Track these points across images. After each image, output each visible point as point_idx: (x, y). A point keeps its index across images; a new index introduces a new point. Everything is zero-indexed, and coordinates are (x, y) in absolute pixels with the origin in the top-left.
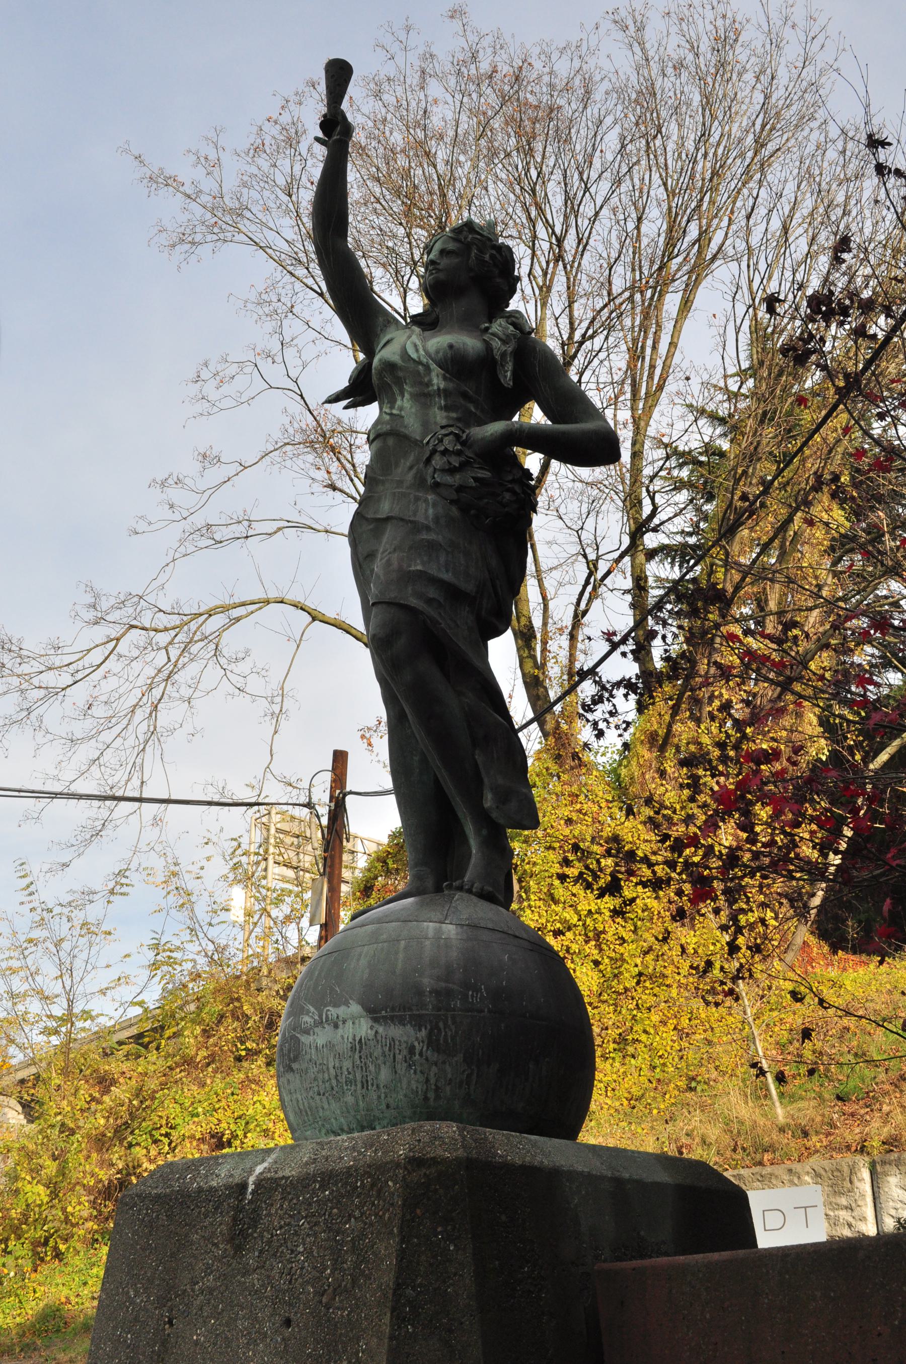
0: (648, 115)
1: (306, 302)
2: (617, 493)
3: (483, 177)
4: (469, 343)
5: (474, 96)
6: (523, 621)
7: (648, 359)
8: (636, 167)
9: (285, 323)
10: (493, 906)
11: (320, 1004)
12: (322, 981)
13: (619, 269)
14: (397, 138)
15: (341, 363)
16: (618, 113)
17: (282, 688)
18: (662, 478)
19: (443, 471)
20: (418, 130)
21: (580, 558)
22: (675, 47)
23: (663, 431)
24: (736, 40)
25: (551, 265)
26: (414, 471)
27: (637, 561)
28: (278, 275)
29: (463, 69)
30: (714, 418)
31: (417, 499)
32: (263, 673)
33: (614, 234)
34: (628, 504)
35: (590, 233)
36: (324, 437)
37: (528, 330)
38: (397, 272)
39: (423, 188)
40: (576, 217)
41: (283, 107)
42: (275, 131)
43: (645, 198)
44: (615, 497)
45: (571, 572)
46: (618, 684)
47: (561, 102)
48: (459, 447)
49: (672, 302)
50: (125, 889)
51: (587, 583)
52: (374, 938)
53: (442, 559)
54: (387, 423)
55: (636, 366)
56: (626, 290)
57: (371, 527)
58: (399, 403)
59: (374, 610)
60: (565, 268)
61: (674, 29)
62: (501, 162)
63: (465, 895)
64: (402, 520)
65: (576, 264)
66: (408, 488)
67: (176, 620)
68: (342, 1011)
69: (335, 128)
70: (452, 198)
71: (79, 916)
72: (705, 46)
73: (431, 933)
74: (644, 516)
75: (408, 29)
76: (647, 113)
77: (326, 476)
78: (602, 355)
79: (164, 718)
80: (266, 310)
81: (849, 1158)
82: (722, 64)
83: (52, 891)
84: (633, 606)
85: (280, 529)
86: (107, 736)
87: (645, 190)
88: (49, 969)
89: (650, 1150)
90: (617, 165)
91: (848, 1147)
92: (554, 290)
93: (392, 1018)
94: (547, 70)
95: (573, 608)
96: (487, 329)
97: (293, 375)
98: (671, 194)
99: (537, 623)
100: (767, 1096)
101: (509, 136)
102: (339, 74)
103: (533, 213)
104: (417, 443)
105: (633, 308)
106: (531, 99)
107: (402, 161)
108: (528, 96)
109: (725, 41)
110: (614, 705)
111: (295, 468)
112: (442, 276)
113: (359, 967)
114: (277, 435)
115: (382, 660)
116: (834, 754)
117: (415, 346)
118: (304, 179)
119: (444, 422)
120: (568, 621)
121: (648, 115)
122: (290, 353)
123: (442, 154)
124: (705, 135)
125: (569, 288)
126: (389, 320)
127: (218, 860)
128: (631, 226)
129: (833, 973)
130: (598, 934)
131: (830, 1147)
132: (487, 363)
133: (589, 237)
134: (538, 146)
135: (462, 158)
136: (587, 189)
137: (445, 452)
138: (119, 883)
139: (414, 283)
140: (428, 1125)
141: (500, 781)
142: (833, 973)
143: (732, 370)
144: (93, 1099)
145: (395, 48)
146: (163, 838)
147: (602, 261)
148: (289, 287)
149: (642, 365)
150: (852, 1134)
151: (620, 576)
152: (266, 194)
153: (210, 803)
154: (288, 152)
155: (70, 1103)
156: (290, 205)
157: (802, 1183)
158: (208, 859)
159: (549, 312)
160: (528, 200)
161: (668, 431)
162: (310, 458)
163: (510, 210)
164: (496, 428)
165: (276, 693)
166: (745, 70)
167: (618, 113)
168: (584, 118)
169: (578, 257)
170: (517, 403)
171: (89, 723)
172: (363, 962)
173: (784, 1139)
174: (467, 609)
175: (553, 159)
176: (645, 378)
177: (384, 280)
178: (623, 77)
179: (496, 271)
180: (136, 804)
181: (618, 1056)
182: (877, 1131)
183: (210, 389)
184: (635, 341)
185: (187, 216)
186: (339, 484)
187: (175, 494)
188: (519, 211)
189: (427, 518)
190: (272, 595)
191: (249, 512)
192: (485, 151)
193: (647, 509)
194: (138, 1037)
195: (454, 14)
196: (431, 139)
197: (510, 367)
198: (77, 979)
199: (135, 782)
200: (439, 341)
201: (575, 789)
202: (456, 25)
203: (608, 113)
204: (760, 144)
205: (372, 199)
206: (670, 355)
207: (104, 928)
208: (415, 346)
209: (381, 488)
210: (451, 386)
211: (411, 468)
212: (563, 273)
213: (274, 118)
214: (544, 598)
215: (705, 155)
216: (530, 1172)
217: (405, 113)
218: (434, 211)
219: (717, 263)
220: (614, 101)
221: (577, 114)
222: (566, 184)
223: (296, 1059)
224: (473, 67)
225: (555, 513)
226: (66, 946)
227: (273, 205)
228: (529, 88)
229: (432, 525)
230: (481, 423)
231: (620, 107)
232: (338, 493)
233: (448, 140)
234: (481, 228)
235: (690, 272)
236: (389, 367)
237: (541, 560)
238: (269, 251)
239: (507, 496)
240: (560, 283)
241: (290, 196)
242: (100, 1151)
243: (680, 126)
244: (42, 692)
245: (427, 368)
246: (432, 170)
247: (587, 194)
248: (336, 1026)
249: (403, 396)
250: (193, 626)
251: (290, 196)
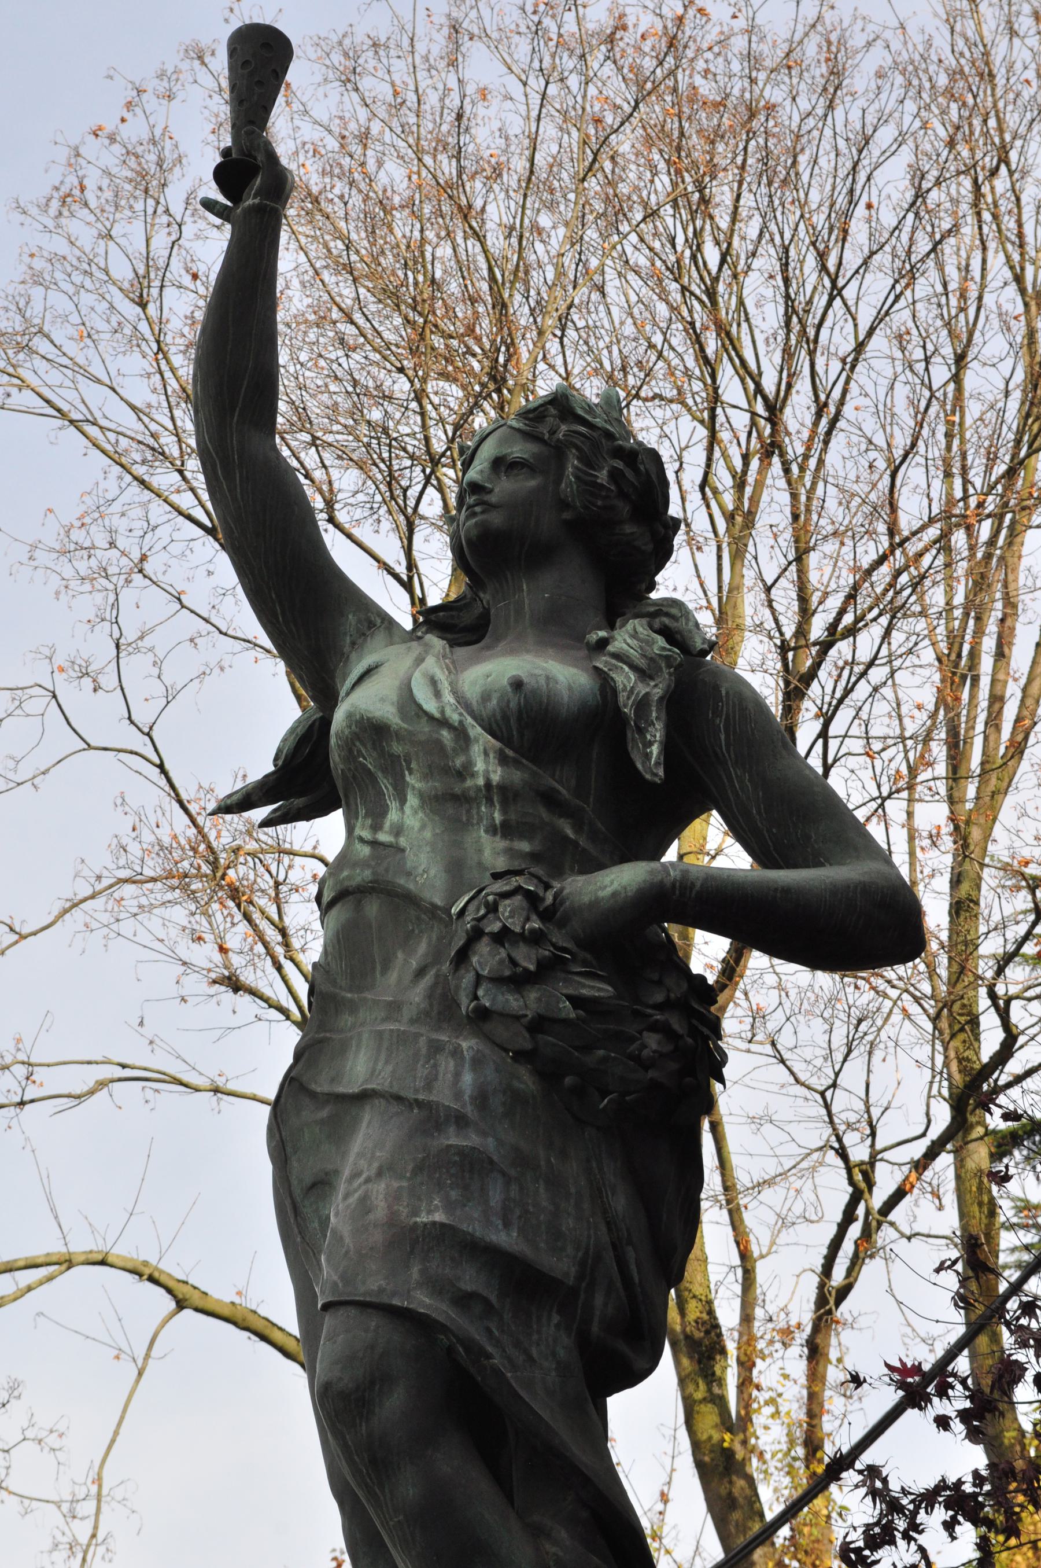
0: (977, 122)
1: (175, 549)
2: (917, 1000)
3: (594, 263)
4: (563, 675)
5: (574, 81)
6: (694, 1311)
7: (985, 682)
8: (952, 240)
13: (913, 474)
15: (259, 708)
16: (907, 119)
17: (99, 1480)
18: (1026, 959)
19: (497, 980)
20: (443, 158)
21: (831, 1157)
23: (1026, 853)
25: (755, 464)
26: (428, 979)
27: (971, 1165)
28: (111, 487)
29: (547, 22)
31: (436, 1048)
32: (53, 1440)
33: (901, 392)
34: (944, 1024)
35: (845, 392)
36: (214, 864)
37: (699, 645)
38: (391, 479)
39: (454, 287)
40: (812, 353)
41: (129, 105)
42: (111, 157)
43: (972, 311)
44: (914, 1009)
45: (808, 1194)
46: (928, 1499)
47: (775, 94)
48: (536, 924)
51: (849, 1217)
53: (496, 1197)
54: (364, 864)
55: (957, 699)
56: (931, 521)
57: (324, 1113)
58: (393, 816)
59: (329, 1321)
60: (787, 471)
62: (635, 229)
64: (398, 1098)
65: (812, 463)
66: (412, 1021)
70: (521, 312)
74: (985, 1058)
77: (217, 957)
78: (877, 674)
80: (83, 567)
84: (962, 1300)
85: (102, 1084)
87: (973, 294)
90: (905, 238)
92: (762, 521)
94: (741, 23)
95: (815, 1280)
96: (602, 644)
99: (728, 1316)
101: (655, 174)
102: (260, 60)
103: (712, 345)
104: (436, 914)
105: (948, 565)
106: (706, 89)
107: (403, 226)
108: (698, 80)
110: (922, 1550)
111: (144, 937)
112: (496, 519)
114: (102, 861)
115: (345, 1447)
117: (433, 682)
118: (176, 265)
119: (501, 864)
120: (804, 1313)
121: (977, 122)
122: (135, 666)
123: (497, 212)
125: (796, 517)
126: (376, 620)
128: (940, 374)
132: (603, 722)
133: (842, 402)
134: (722, 194)
135: (545, 220)
136: (836, 292)
137: (503, 936)
139: (432, 505)
147: (873, 455)
148: (137, 512)
149: (973, 696)
151: (927, 1204)
152: (87, 299)
154: (139, 206)
156: (144, 327)
159: (749, 576)
160: (700, 316)
162: (179, 914)
163: (658, 339)
164: (623, 878)
165: (81, 1493)
167: (907, 119)
168: (828, 132)
169: (818, 445)
170: (675, 823)
174: (556, 1318)
175: (756, 223)
176: (980, 727)
177: (361, 497)
178: (918, 39)
179: (624, 509)
184: (954, 639)
186: (247, 977)
188: (679, 339)
189: (458, 1095)
190: (81, 1244)
191: (27, 1044)
192: (599, 206)
196: (473, 178)
197: (657, 732)
200: (491, 671)
203: (883, 119)
205: (335, 314)
208: (433, 682)
209: (347, 1020)
210: (517, 776)
211: (420, 973)
212: (782, 483)
213: (109, 127)
214: (745, 1255)
217: (412, 119)
218: (478, 340)
220: (898, 92)
221: (811, 122)
222: (787, 281)
224: (570, 17)
225: (768, 1049)
227: (101, 326)
228: (701, 65)
229: (469, 1110)
230: (591, 865)
231: (910, 106)
232: (244, 1000)
233: (511, 180)
234: (590, 408)
236: (372, 731)
237: (736, 1160)
238: (93, 431)
239: (653, 1041)
240: (774, 507)
241: (143, 305)
245: (461, 733)
246: (474, 247)
247: (838, 302)
249: (403, 801)
251: (143, 305)
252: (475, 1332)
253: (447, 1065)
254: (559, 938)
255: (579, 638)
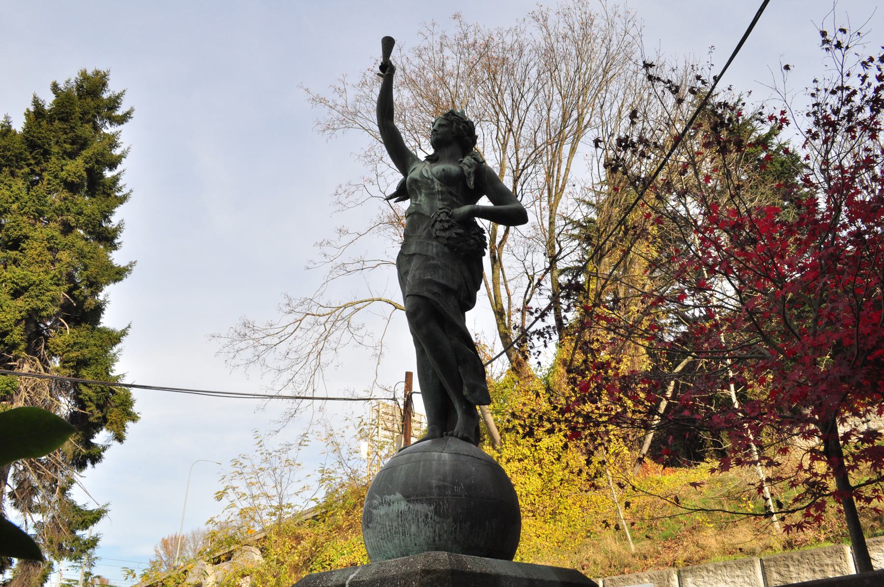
4: (453, 168)
9: (378, 165)
10: (468, 444)
11: (382, 494)
12: (385, 482)
13: (539, 134)
14: (430, 76)
15: (394, 178)
19: (440, 230)
22: (563, 28)
24: (592, 24)
30: (590, 204)
31: (428, 244)
39: (444, 99)
49: (566, 149)
50: (306, 443)
51: (529, 286)
52: (408, 461)
59: (408, 299)
61: (562, 20)
63: (453, 438)
67: (329, 310)
68: (392, 497)
69: (387, 69)
71: (284, 457)
72: (577, 27)
73: (436, 458)
75: (434, 25)
76: (550, 59)
78: (532, 176)
79: (324, 358)
81: (667, 569)
82: (585, 35)
83: (273, 444)
86: (296, 368)
88: (270, 482)
89: (568, 567)
91: (667, 564)
93: (417, 500)
97: (383, 190)
98: (564, 97)
99: (505, 306)
100: (626, 539)
102: (388, 44)
109: (586, 24)
112: (439, 137)
113: (401, 475)
116: (655, 369)
122: (381, 179)
123: (452, 82)
124: (578, 69)
127: (352, 428)
128: (544, 113)
129: (659, 477)
130: (540, 461)
131: (657, 564)
132: (461, 177)
134: (498, 77)
135: (462, 84)
136: (523, 96)
137: (441, 221)
138: (303, 440)
140: (432, 553)
141: (471, 381)
142: (659, 477)
143: (596, 181)
144: (293, 547)
145: (428, 34)
146: (325, 417)
150: (668, 557)
152: (368, 104)
153: (345, 399)
155: (281, 549)
157: (644, 582)
158: (347, 427)
161: (565, 211)
162: (392, 230)
164: (466, 208)
166: (596, 38)
171: (287, 362)
172: (403, 473)
173: (635, 561)
180: (311, 401)
181: (552, 521)
182: (681, 555)
183: (342, 198)
184: (549, 168)
185: (330, 116)
187: (326, 249)
190: (375, 297)
193: (557, 249)
194: (314, 518)
195: (455, 17)
197: (472, 179)
198: (284, 488)
199: (310, 390)
200: (438, 168)
201: (526, 388)
202: (457, 22)
204: (605, 72)
206: (566, 175)
207: (297, 462)
209: (411, 240)
210: (444, 189)
214: (509, 295)
215: (579, 79)
216: (484, 576)
219: (588, 129)
223: (370, 522)
226: (278, 471)
230: (459, 206)
235: (574, 134)
236: (414, 181)
239: (472, 241)
240: (511, 142)
242: (296, 573)
243: (566, 65)
244: (265, 347)
245: (432, 180)
248: (389, 505)
250: (337, 313)
252: (437, 300)
253: (430, 247)
254: (453, 221)
255: (456, 160)
